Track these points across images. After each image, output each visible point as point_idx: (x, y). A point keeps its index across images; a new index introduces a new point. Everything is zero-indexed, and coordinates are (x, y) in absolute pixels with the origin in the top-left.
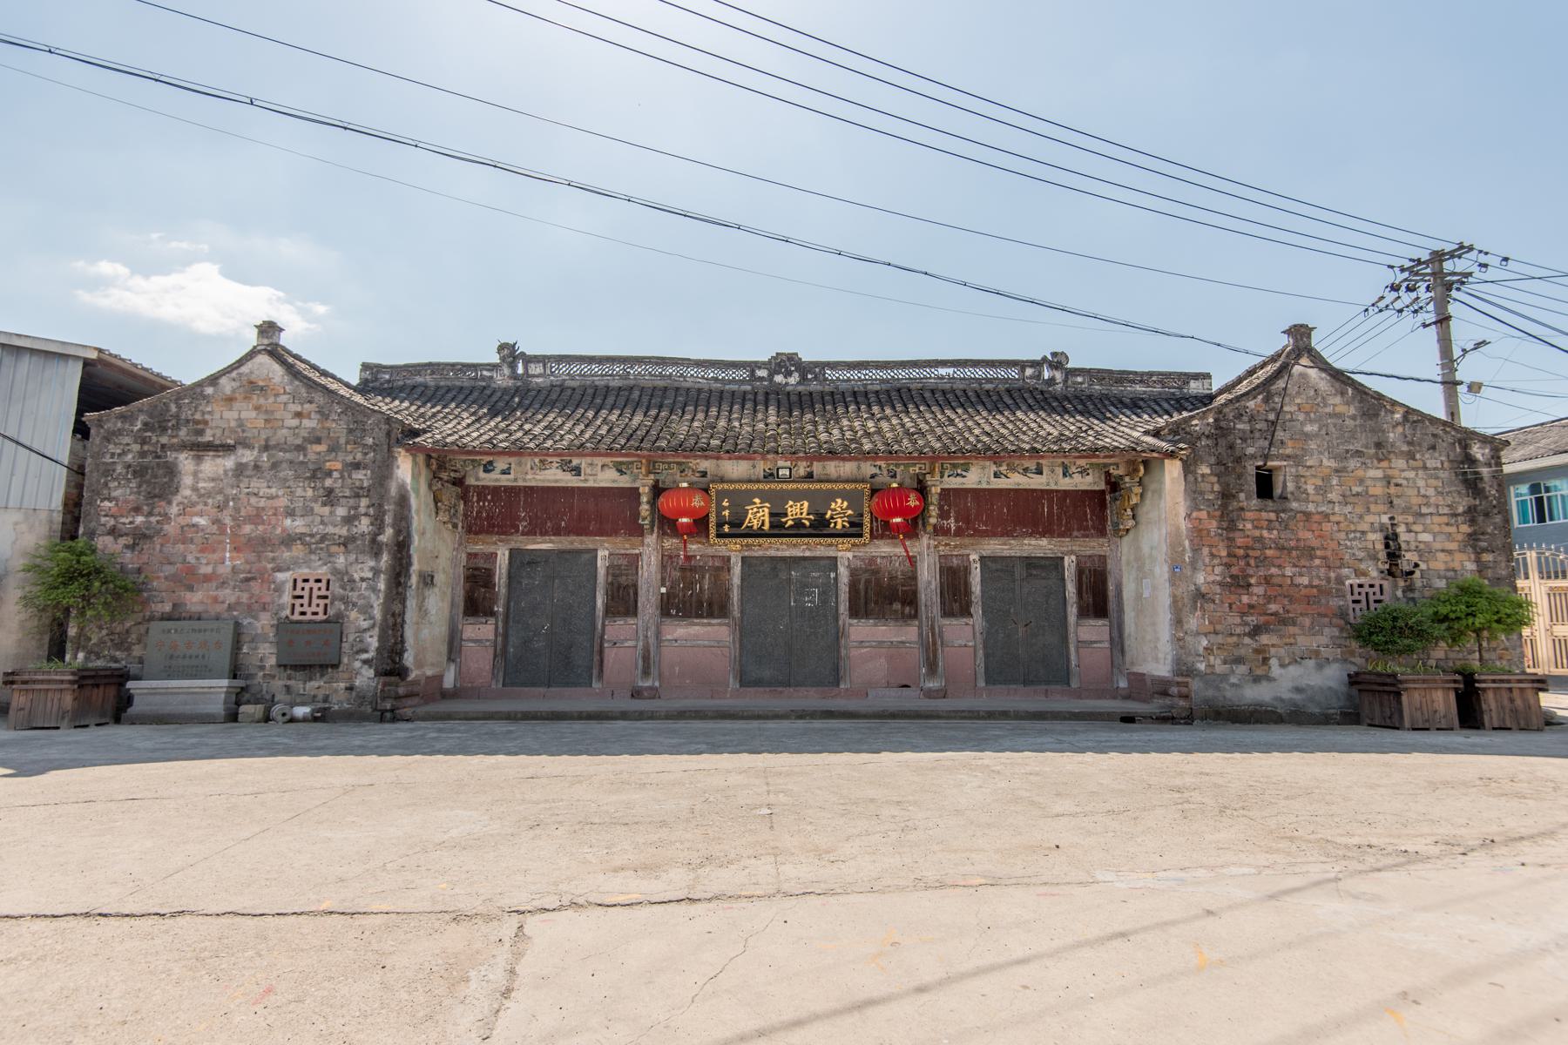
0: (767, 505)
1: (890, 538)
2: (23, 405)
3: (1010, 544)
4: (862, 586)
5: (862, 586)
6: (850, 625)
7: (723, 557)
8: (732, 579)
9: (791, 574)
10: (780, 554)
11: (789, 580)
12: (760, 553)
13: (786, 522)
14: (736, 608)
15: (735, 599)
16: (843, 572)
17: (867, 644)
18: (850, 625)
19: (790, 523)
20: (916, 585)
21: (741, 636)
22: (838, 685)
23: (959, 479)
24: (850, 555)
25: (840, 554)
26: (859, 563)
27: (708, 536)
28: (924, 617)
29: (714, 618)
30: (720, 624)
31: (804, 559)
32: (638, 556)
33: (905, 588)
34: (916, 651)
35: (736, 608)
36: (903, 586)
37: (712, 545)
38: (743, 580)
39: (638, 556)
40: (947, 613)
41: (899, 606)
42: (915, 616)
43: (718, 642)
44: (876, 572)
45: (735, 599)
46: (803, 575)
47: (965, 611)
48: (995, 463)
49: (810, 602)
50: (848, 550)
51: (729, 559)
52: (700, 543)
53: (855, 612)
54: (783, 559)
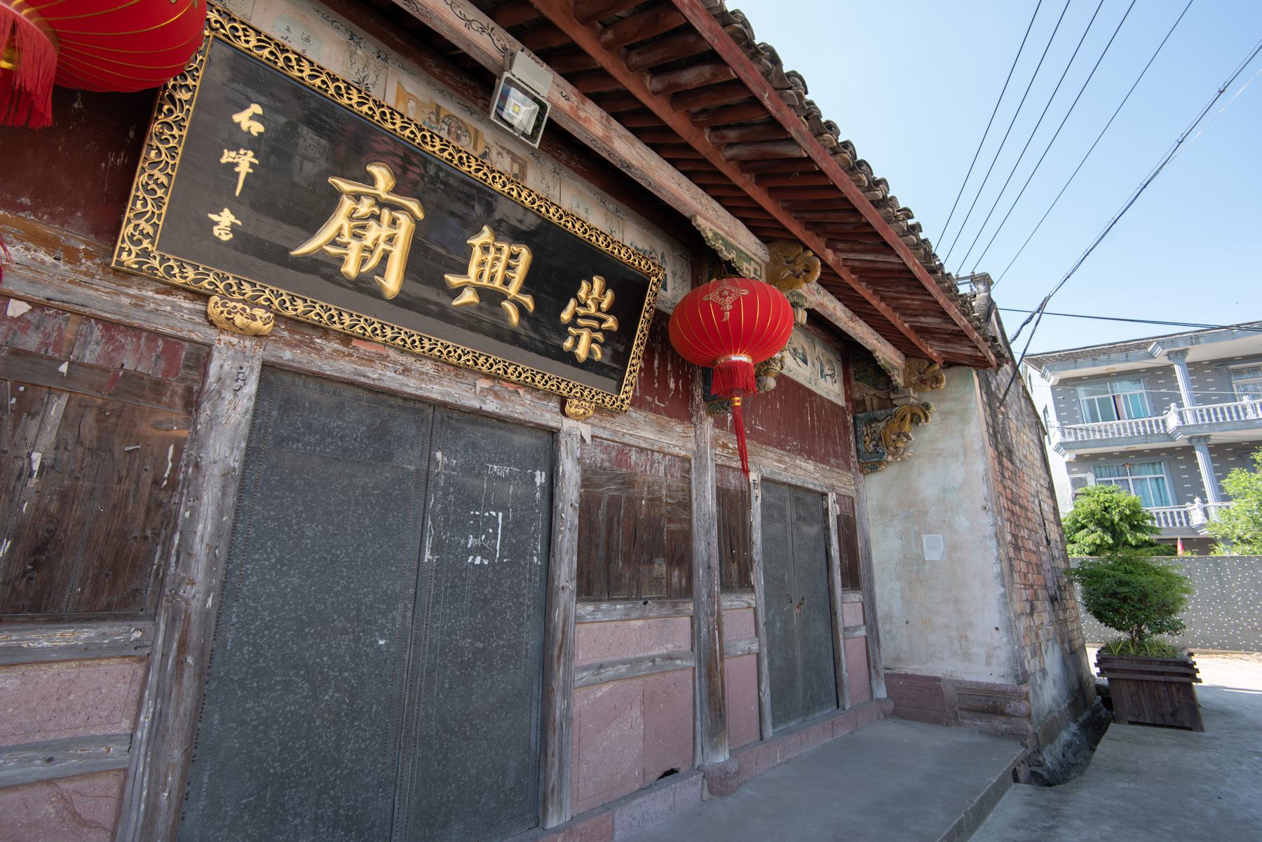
0: (414, 206)
1: (651, 410)
2: (1025, 350)
3: (786, 463)
4: (601, 515)
5: (601, 515)
6: (579, 620)
7: (173, 342)
8: (198, 440)
9: (431, 459)
10: (411, 386)
11: (425, 478)
12: (344, 367)
13: (458, 291)
14: (199, 569)
15: (204, 528)
16: (569, 470)
17: (610, 672)
18: (579, 620)
19: (468, 297)
20: (690, 521)
21: (202, 698)
22: (539, 821)
23: (368, 350)
24: (586, 431)
25: (567, 424)
26: (600, 456)
27: (109, 230)
28: (704, 591)
29: (57, 620)
30: (85, 654)
31: (478, 416)
32: (391, 251)
33: (673, 527)
34: (689, 674)
35: (199, 569)
36: (670, 521)
37: (123, 274)
38: (251, 454)
39: (391, 251)
40: (727, 587)
41: (664, 569)
42: (687, 591)
43: (49, 752)
44: (627, 482)
45: (204, 528)
46: (467, 469)
47: (745, 584)
48: (89, 344)
49: (478, 550)
50: (583, 418)
51: (201, 356)
52: (50, 244)
53: (587, 589)
54: (416, 404)
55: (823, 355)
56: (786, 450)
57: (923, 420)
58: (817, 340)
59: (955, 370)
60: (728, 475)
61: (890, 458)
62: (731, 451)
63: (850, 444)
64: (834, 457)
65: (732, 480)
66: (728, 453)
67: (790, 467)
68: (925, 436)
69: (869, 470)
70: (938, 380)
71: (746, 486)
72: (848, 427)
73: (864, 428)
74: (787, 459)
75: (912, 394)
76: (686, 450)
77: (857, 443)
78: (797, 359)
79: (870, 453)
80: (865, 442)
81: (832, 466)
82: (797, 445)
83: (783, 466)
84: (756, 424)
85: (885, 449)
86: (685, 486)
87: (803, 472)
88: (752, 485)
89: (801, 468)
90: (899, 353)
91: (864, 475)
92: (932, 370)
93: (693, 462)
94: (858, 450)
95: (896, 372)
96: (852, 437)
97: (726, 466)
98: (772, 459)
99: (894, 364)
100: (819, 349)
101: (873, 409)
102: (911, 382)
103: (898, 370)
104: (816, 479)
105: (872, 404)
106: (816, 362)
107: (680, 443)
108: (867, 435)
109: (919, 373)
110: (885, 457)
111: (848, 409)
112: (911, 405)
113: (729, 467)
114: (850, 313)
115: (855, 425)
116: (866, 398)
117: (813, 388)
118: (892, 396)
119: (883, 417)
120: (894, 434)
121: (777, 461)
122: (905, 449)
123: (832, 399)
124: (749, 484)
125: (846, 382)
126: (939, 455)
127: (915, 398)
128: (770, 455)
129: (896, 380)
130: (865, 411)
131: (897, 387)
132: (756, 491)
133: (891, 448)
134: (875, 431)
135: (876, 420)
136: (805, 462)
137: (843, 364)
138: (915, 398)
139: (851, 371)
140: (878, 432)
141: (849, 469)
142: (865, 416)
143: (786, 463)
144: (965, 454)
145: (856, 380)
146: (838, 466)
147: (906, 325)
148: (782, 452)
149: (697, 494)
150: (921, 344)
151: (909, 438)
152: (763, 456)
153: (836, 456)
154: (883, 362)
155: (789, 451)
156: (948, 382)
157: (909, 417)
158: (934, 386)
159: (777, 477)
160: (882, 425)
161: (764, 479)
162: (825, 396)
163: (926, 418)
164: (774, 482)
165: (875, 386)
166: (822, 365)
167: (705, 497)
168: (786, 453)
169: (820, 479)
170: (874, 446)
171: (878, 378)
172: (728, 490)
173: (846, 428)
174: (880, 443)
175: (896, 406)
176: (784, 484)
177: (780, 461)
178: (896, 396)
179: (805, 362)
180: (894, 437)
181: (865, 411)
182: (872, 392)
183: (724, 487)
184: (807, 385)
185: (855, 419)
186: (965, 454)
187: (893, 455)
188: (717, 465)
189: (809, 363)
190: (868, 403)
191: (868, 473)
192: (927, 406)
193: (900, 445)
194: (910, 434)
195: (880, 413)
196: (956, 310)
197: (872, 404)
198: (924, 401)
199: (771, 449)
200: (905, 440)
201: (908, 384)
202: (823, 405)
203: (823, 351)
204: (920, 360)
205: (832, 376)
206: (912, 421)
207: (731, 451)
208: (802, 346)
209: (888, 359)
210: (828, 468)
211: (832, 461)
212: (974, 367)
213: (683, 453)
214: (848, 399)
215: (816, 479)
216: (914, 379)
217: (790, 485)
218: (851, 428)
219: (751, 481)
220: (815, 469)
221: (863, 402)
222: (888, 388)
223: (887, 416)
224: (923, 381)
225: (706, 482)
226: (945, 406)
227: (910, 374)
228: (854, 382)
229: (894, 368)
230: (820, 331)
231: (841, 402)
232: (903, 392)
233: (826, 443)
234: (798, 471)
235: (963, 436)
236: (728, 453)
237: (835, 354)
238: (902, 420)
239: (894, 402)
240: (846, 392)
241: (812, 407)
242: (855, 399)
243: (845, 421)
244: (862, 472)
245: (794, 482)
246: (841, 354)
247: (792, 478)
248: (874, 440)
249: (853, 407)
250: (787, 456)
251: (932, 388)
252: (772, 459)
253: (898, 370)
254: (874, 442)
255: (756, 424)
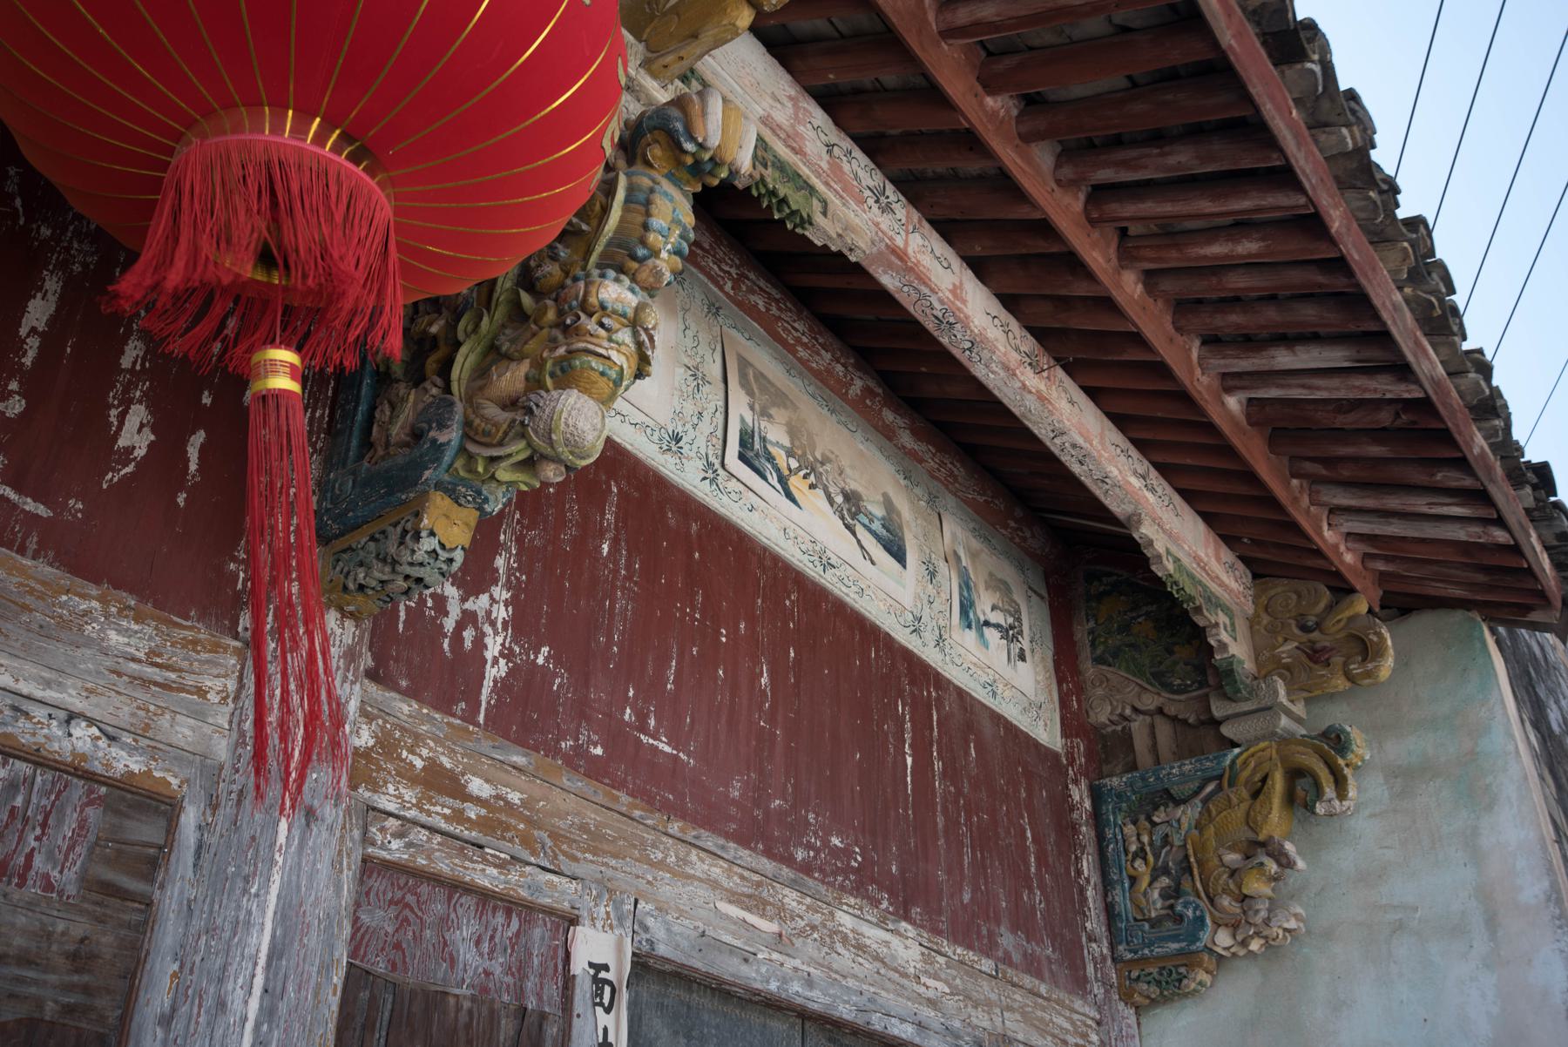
3: (781, 913)
55: (974, 556)
56: (789, 860)
57: (1329, 791)
58: (950, 501)
59: (1423, 624)
60: (444, 922)
61: (1223, 939)
62: (472, 812)
63: (1082, 891)
64: (1014, 928)
65: (468, 955)
66: (458, 817)
67: (801, 933)
68: (1344, 859)
69: (1154, 991)
70: (1367, 650)
71: (553, 991)
72: (1074, 828)
73: (1130, 829)
74: (791, 898)
75: (1282, 696)
76: (153, 753)
77: (1107, 885)
78: (859, 529)
79: (1155, 923)
80: (1133, 880)
81: (1007, 960)
82: (847, 853)
83: (770, 927)
84: (643, 728)
85: (1204, 903)
86: (106, 941)
87: (869, 966)
88: (583, 989)
89: (861, 948)
90: (1227, 555)
91: (1138, 1010)
92: (1347, 614)
93: (190, 818)
94: (1110, 912)
95: (1222, 618)
96: (1087, 865)
97: (435, 879)
98: (714, 885)
99: (1214, 587)
100: (956, 533)
101: (1157, 761)
102: (1277, 660)
103: (1227, 611)
104: (932, 1003)
105: (1154, 748)
106: (943, 567)
107: (119, 708)
108: (1139, 852)
109: (1305, 629)
110: (1205, 937)
111: (1072, 762)
112: (1286, 740)
113: (456, 887)
114: (1029, 343)
115: (1097, 817)
116: (1135, 726)
117: (931, 656)
118: (1218, 709)
119: (1194, 785)
120: (1232, 849)
121: (735, 898)
122: (1274, 905)
123: (1011, 711)
124: (569, 982)
125: (1065, 666)
126: (1399, 927)
127: (1298, 720)
128: (700, 865)
129: (1223, 646)
130: (1133, 767)
131: (1230, 672)
132: (604, 1019)
133: (1226, 902)
134: (1166, 840)
135: (1169, 798)
136: (881, 924)
137: (1051, 606)
138: (1298, 720)
139: (1081, 632)
140: (1177, 840)
141: (1079, 984)
142: (1131, 784)
143: (781, 913)
144: (1492, 922)
145: (1099, 660)
146: (1032, 966)
147: (1233, 403)
148: (768, 865)
149: (180, 993)
150: (1296, 500)
151: (1285, 862)
152: (661, 865)
153: (1022, 922)
154: (1170, 567)
155: (806, 868)
156: (1403, 662)
157: (1278, 783)
158: (1355, 668)
159: (730, 968)
160: (1188, 814)
161: (643, 966)
162: (981, 695)
163: (1340, 783)
164: (721, 990)
165: (1160, 679)
166: (966, 585)
167: (221, 1005)
168: (786, 872)
169: (951, 1003)
170: (1165, 895)
171: (1170, 652)
172: (435, 1000)
173: (1067, 830)
174: (1186, 885)
175: (1234, 745)
176: (773, 1005)
177: (756, 903)
178: (1232, 709)
179: (899, 556)
180: (1232, 858)
181: (1133, 767)
182: (1150, 701)
183: (411, 978)
184: (903, 637)
185: (1096, 795)
186: (1492, 922)
187: (1234, 927)
188: (370, 867)
189: (912, 557)
190: (1141, 743)
191: (1154, 1003)
192: (1336, 741)
193: (1256, 886)
194: (1289, 847)
195: (1179, 771)
196: (1398, 297)
197: (1154, 748)
198: (1324, 727)
199: (710, 841)
200: (1272, 867)
201: (1269, 666)
202: (969, 727)
203: (976, 544)
204: (1301, 586)
205: (1010, 633)
206: (1290, 799)
207: (472, 812)
208: (886, 496)
209: (1186, 561)
210: (987, 965)
211: (1007, 940)
212: (1492, 618)
213: (125, 761)
214: (1071, 725)
215: (932, 1003)
216: (1287, 650)
217: (805, 1016)
218: (1086, 832)
219: (579, 966)
220: (926, 960)
221: (1126, 739)
222: (1203, 684)
223: (1206, 781)
224: (1316, 655)
225: (243, 925)
226: (1401, 749)
227: (1272, 631)
228: (1089, 670)
229: (1218, 604)
230: (960, 471)
231: (1047, 732)
232: (1253, 692)
233: (980, 867)
234: (845, 959)
235: (1476, 856)
236: (458, 817)
237: (1021, 568)
238: (1255, 795)
239: (1226, 730)
240: (1064, 704)
241: (921, 725)
242: (1096, 729)
243: (1062, 805)
244: (1127, 997)
245: (817, 1000)
246: (1047, 576)
247: (809, 982)
248: (1165, 871)
249: (1090, 754)
250: (793, 885)
251: (1349, 677)
252: (714, 885)
253: (1227, 611)
254: (1165, 881)
255: (643, 728)
